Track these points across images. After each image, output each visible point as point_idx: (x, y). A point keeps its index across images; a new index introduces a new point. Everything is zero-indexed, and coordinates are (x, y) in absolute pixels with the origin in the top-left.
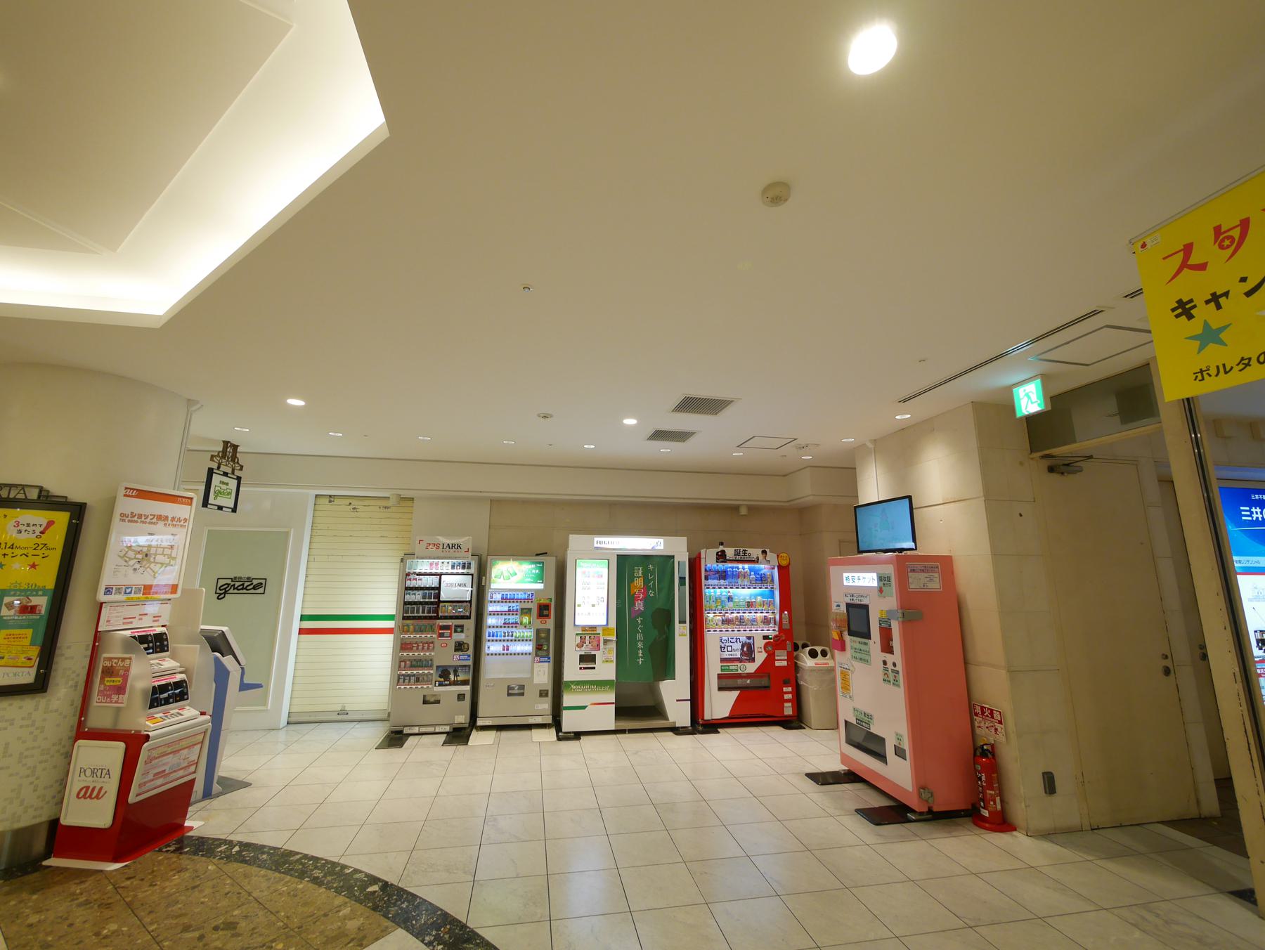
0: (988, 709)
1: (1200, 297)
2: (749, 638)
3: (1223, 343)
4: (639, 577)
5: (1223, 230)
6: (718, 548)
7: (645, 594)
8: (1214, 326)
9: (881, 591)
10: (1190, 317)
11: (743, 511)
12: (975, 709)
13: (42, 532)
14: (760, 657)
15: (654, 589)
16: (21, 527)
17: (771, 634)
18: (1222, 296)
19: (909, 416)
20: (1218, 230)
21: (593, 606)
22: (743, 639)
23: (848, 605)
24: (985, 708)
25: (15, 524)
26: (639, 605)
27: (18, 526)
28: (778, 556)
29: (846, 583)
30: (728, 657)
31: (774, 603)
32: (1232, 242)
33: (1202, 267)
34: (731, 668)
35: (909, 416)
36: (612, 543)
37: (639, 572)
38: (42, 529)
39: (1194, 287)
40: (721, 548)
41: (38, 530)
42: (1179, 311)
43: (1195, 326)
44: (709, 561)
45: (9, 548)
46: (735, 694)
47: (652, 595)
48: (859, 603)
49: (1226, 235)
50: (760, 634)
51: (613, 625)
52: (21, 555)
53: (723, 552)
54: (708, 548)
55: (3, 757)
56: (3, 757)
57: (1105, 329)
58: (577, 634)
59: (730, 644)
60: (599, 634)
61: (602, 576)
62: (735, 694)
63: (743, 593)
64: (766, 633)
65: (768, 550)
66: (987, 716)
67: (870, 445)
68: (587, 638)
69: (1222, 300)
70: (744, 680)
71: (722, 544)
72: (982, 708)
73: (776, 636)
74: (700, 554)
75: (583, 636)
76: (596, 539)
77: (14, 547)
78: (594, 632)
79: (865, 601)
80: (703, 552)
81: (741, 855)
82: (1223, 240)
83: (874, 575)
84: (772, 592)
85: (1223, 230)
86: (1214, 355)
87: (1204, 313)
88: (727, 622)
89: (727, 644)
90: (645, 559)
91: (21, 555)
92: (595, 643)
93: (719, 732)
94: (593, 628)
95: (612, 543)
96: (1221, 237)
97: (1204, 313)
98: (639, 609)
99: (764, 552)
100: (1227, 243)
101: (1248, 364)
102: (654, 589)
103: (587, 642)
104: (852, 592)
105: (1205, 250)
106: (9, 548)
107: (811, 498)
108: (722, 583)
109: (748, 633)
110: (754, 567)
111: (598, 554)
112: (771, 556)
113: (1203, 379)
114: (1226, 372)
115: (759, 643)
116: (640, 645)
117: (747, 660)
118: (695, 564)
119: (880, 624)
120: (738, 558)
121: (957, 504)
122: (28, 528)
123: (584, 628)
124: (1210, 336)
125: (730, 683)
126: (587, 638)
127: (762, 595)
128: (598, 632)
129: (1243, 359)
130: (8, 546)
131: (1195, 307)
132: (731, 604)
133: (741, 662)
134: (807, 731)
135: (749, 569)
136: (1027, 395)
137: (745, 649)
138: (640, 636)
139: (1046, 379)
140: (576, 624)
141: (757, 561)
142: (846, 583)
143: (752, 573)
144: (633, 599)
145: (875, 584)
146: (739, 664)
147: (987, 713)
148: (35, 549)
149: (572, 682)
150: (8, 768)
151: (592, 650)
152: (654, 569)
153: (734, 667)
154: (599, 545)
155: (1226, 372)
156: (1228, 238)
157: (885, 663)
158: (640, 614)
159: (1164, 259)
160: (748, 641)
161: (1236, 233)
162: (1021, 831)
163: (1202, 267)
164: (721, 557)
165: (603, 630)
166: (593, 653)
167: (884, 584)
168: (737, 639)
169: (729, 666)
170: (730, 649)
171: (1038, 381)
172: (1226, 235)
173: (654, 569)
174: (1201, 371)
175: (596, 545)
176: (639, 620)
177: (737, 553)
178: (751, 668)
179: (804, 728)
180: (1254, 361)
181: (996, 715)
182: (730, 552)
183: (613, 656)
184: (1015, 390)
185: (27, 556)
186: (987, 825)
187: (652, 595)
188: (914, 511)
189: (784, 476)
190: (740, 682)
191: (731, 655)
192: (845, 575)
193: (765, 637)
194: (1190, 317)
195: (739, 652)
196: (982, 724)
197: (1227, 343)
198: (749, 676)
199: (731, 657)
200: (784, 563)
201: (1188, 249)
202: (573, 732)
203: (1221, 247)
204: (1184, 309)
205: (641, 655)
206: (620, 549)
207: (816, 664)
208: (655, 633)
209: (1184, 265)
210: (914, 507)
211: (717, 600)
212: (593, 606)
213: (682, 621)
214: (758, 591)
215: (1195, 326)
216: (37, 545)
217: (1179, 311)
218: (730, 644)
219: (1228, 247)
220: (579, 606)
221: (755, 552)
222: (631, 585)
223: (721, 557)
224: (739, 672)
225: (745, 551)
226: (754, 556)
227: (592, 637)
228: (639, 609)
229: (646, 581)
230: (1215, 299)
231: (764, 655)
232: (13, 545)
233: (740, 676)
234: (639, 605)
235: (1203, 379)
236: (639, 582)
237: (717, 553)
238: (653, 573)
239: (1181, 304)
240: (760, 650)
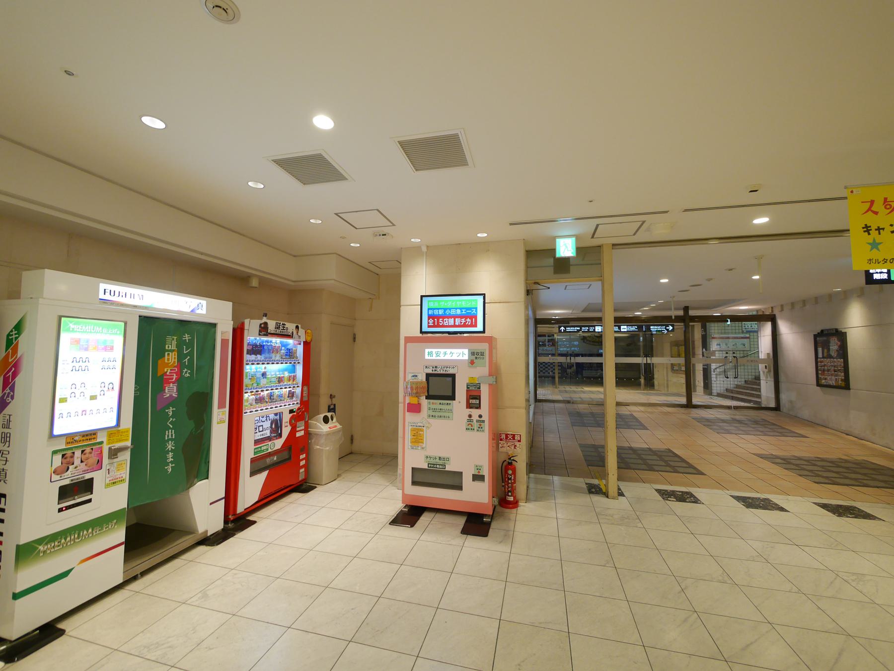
0: (511, 434)
1: (874, 227)
2: (276, 414)
3: (878, 249)
4: (172, 351)
5: (888, 200)
6: (261, 319)
7: (179, 373)
8: (877, 241)
9: (472, 363)
10: (869, 234)
11: (255, 283)
12: (500, 437)
14: (286, 431)
15: (190, 366)
17: (295, 407)
18: (881, 229)
19: (485, 235)
20: (886, 199)
21: (93, 398)
22: (272, 416)
23: (428, 376)
24: (509, 434)
26: (171, 390)
28: (306, 332)
29: (427, 357)
30: (260, 437)
31: (294, 378)
32: (891, 207)
33: (876, 213)
34: (263, 449)
35: (485, 235)
36: (132, 296)
37: (172, 344)
39: (873, 221)
40: (265, 320)
42: (865, 229)
43: (870, 239)
44: (251, 337)
46: (265, 474)
47: (188, 375)
48: (444, 372)
49: (889, 203)
50: (286, 408)
51: (127, 423)
53: (266, 324)
54: (252, 318)
57: (376, 211)
58: (55, 452)
59: (261, 424)
60: (102, 442)
61: (112, 348)
62: (265, 474)
63: (274, 369)
64: (292, 407)
65: (300, 326)
66: (510, 439)
67: (424, 249)
68: (78, 453)
69: (881, 231)
70: (271, 458)
71: (265, 315)
72: (507, 435)
73: (299, 409)
74: (243, 324)
75: (69, 453)
76: (103, 286)
78: (93, 442)
79: (451, 371)
80: (247, 321)
81: (285, 630)
82: (887, 205)
83: (466, 351)
84: (294, 370)
85: (888, 200)
86: (875, 254)
87: (874, 233)
88: (260, 400)
89: (259, 424)
90: (182, 325)
92: (93, 459)
93: (254, 522)
94: (90, 435)
95: (132, 296)
96: (887, 203)
97: (874, 233)
98: (171, 396)
99: (297, 327)
100: (888, 207)
101: (886, 262)
102: (190, 366)
103: (77, 462)
104: (435, 364)
107: (333, 282)
108: (259, 359)
109: (275, 410)
110: (284, 342)
112: (302, 332)
113: (870, 264)
114: (878, 263)
115: (287, 417)
116: (170, 446)
117: (275, 436)
118: (238, 332)
119: (468, 388)
120: (278, 331)
121: (505, 304)
123: (70, 438)
124: (874, 245)
125: (261, 464)
126: (78, 453)
127: (285, 370)
128: (99, 440)
129: (884, 259)
131: (871, 230)
132: (263, 382)
133: (270, 441)
134: (319, 489)
135: (281, 343)
136: (565, 245)
137: (273, 426)
138: (170, 434)
139: (578, 238)
141: (290, 336)
142: (427, 357)
143: (283, 348)
144: (161, 382)
145: (466, 357)
146: (270, 443)
147: (510, 437)
149: (40, 541)
151: (86, 472)
152: (191, 341)
153: (265, 448)
154: (107, 297)
155: (878, 263)
156: (889, 205)
157: (470, 416)
158: (171, 402)
160: (276, 417)
162: (522, 501)
163: (876, 213)
164: (264, 330)
165: (110, 435)
166: (88, 476)
167: (476, 358)
168: (267, 417)
169: (261, 447)
170: (261, 429)
171: (574, 239)
172: (889, 203)
173: (191, 341)
174: (870, 260)
175: (102, 296)
176: (170, 411)
177: (277, 327)
178: (278, 444)
179: (316, 487)
180: (888, 261)
181: (517, 438)
182: (272, 325)
183: (125, 473)
184: (558, 240)
186: (511, 506)
187: (188, 375)
188: (486, 304)
189: (295, 256)
190: (268, 461)
191: (263, 435)
192: (427, 351)
193: (291, 411)
194: (869, 234)
195: (269, 430)
196: (505, 445)
197: (872, 251)
198: (276, 452)
199: (262, 437)
200: (309, 339)
201: (872, 202)
202: (36, 630)
203: (886, 208)
204: (867, 229)
205: (171, 459)
206: (146, 308)
207: (330, 428)
208: (190, 425)
209: (869, 209)
210: (486, 302)
211: (253, 377)
212: (93, 398)
213: (222, 405)
214: (284, 366)
215: (870, 239)
217: (865, 229)
218: (261, 424)
219: (888, 209)
220: (64, 400)
221: (291, 327)
222: (160, 362)
223: (264, 330)
224: (270, 450)
225: (284, 325)
226: (290, 331)
227: (88, 450)
228: (171, 396)
229: (181, 357)
230: (879, 229)
231: (289, 428)
233: (270, 455)
234: (171, 390)
235: (870, 264)
236: (171, 358)
237: (261, 324)
238: (190, 345)
240: (286, 424)
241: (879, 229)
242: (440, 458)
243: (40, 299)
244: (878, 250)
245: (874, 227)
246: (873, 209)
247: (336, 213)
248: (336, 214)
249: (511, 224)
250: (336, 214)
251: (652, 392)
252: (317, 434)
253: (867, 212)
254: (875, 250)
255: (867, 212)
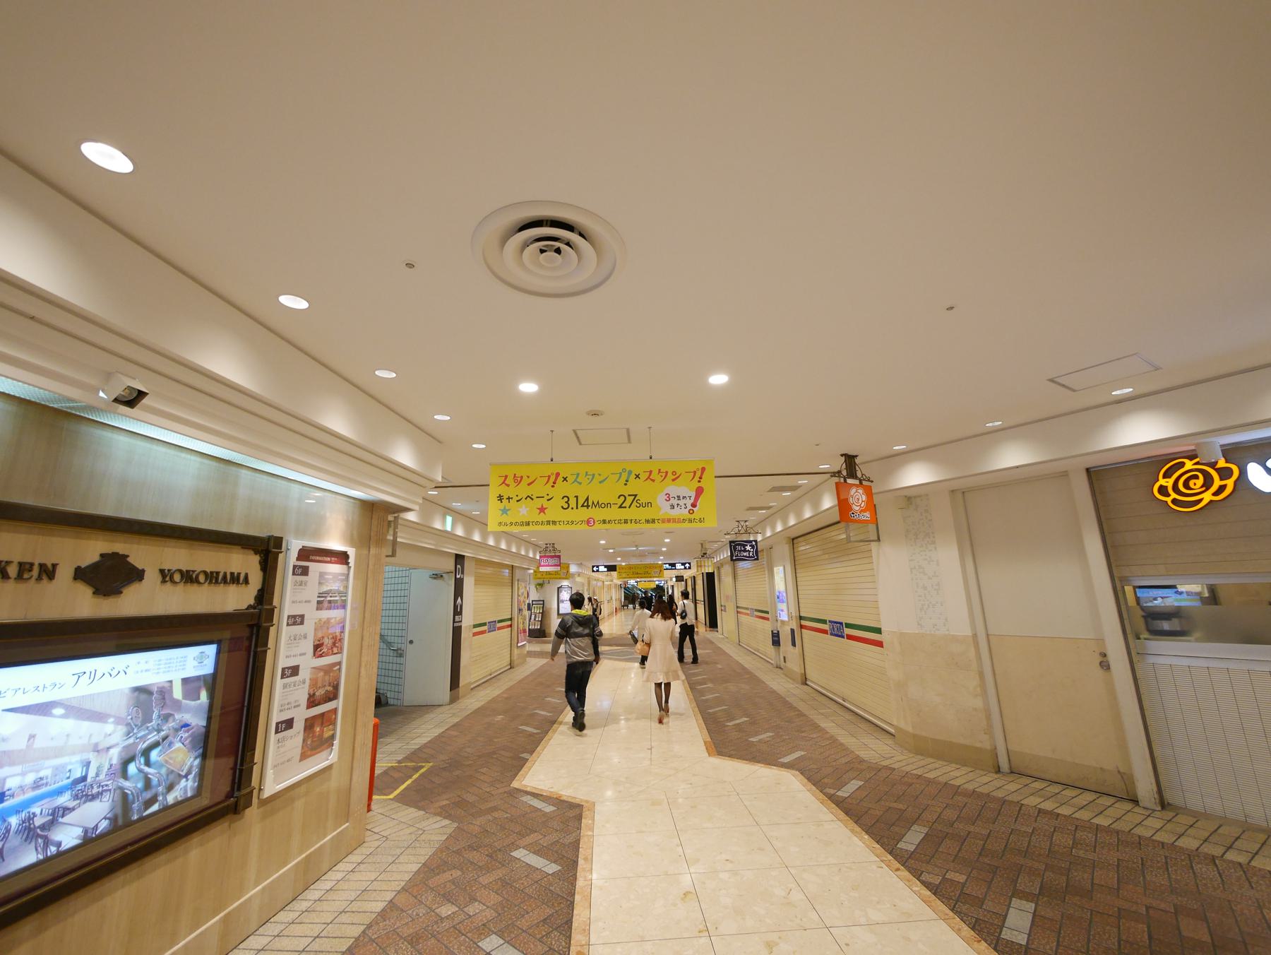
1: (505, 497)
13: (694, 505)
16: (675, 502)
19: (1131, 390)
20: (515, 475)
25: (666, 497)
27: (670, 499)
33: (508, 485)
38: (692, 501)
39: (506, 492)
41: (689, 502)
45: (583, 506)
52: (526, 499)
55: (162, 571)
56: (162, 571)
77: (590, 503)
87: (505, 501)
91: (526, 499)
97: (505, 501)
105: (510, 481)
106: (583, 506)
111: (1203, 588)
122: (679, 502)
124: (505, 511)
130: (580, 503)
140: (561, 612)
148: (620, 507)
150: (713, 623)
159: (716, 477)
161: (519, 479)
163: (508, 485)
185: (532, 499)
194: (502, 502)
204: (500, 498)
215: (502, 506)
216: (622, 498)
232: (587, 499)
239: (500, 496)
241: (509, 498)
242: (679, 497)
243: (1033, 905)
244: (509, 510)
245: (505, 497)
246: (578, 480)
247: (1050, 377)
248: (1052, 380)
249: (716, 477)
250: (1052, 380)
251: (483, 571)
252: (79, 839)
253: (647, 479)
254: (540, 507)
255: (647, 479)
